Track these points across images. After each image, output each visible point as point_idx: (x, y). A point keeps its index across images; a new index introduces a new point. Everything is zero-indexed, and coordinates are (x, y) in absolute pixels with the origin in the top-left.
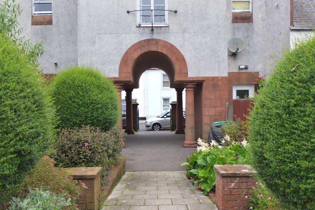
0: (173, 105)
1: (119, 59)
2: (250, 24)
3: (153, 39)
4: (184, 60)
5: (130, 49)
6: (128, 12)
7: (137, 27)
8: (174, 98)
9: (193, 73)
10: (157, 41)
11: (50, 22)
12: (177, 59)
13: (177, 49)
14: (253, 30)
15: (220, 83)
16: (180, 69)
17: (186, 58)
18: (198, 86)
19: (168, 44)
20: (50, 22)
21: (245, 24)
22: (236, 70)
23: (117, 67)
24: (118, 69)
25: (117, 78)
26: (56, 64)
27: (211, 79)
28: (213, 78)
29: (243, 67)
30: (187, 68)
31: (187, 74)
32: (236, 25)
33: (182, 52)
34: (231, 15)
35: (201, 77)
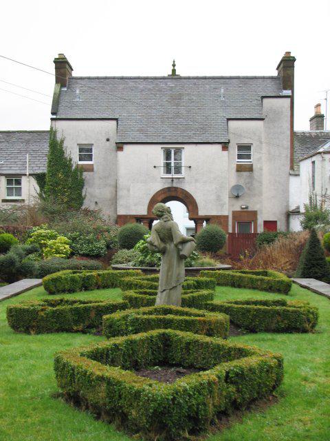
6: (155, 167)
10: (176, 189)
17: (198, 200)
22: (239, 209)
26: (96, 202)
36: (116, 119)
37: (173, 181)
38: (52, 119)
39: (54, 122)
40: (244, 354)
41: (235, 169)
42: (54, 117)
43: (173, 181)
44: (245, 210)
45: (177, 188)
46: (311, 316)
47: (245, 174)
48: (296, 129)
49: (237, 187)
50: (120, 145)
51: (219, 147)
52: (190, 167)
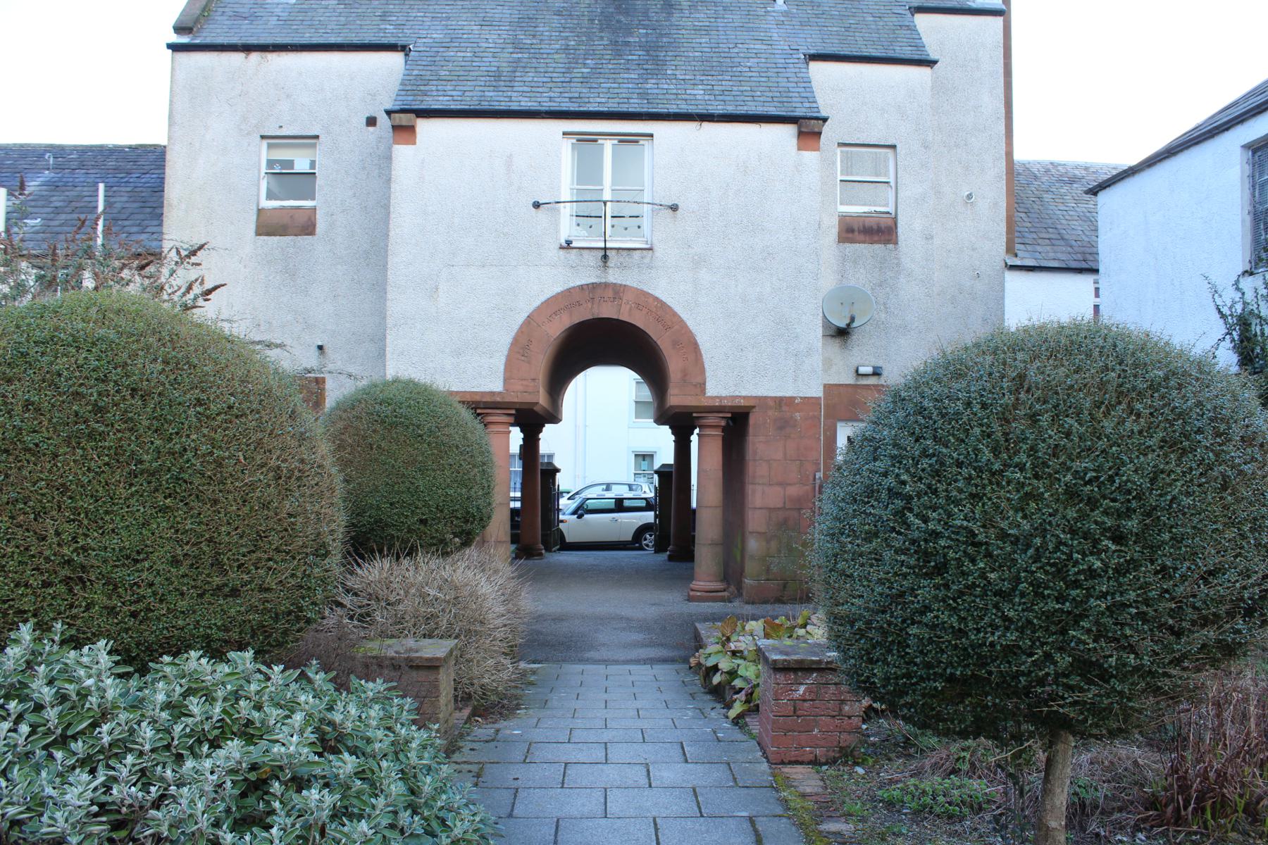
0: (664, 474)
1: (504, 339)
2: (891, 246)
3: (606, 285)
4: (695, 347)
5: (538, 309)
6: (537, 205)
7: (562, 248)
8: (666, 454)
9: (723, 382)
10: (618, 291)
11: (308, 228)
12: (675, 343)
13: (675, 314)
14: (898, 265)
15: (798, 416)
16: (685, 374)
18: (736, 423)
19: (651, 300)
20: (308, 228)
21: (876, 246)
22: (849, 379)
23: (499, 362)
24: (502, 368)
25: (500, 393)
26: (320, 348)
27: (771, 403)
28: (781, 402)
29: (869, 370)
30: (702, 371)
31: (702, 386)
32: (850, 248)
33: (691, 324)
34: (835, 221)
35: (744, 397)
36: (403, 48)
37: (605, 257)
38: (175, 48)
39: (183, 57)
40: (649, 539)
41: (834, 232)
42: (185, 40)
43: (605, 257)
44: (872, 381)
45: (625, 287)
46: (328, 729)
47: (865, 250)
48: (1019, 155)
49: (844, 295)
50: (404, 119)
51: (789, 131)
52: (674, 208)
